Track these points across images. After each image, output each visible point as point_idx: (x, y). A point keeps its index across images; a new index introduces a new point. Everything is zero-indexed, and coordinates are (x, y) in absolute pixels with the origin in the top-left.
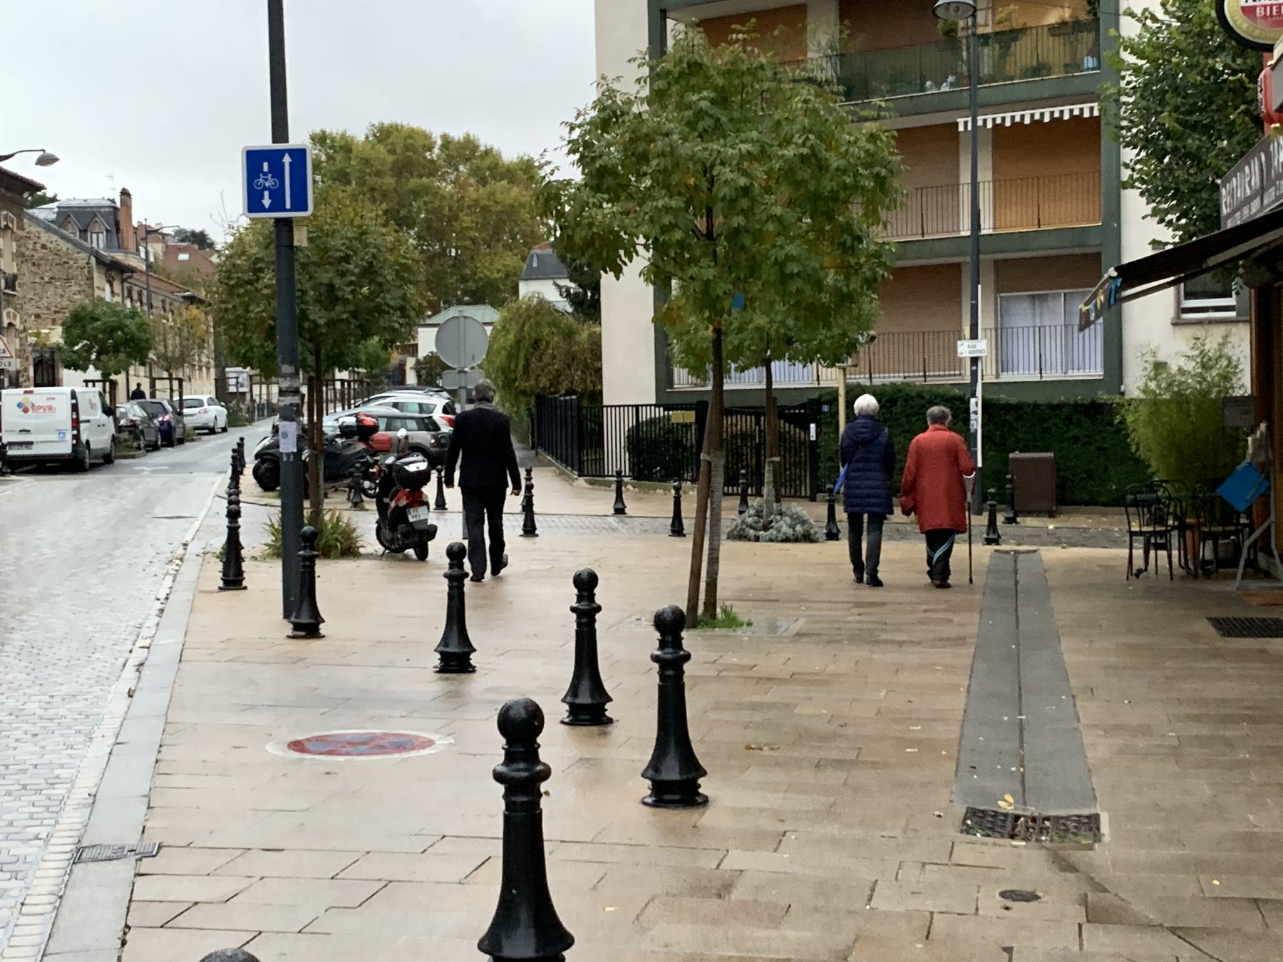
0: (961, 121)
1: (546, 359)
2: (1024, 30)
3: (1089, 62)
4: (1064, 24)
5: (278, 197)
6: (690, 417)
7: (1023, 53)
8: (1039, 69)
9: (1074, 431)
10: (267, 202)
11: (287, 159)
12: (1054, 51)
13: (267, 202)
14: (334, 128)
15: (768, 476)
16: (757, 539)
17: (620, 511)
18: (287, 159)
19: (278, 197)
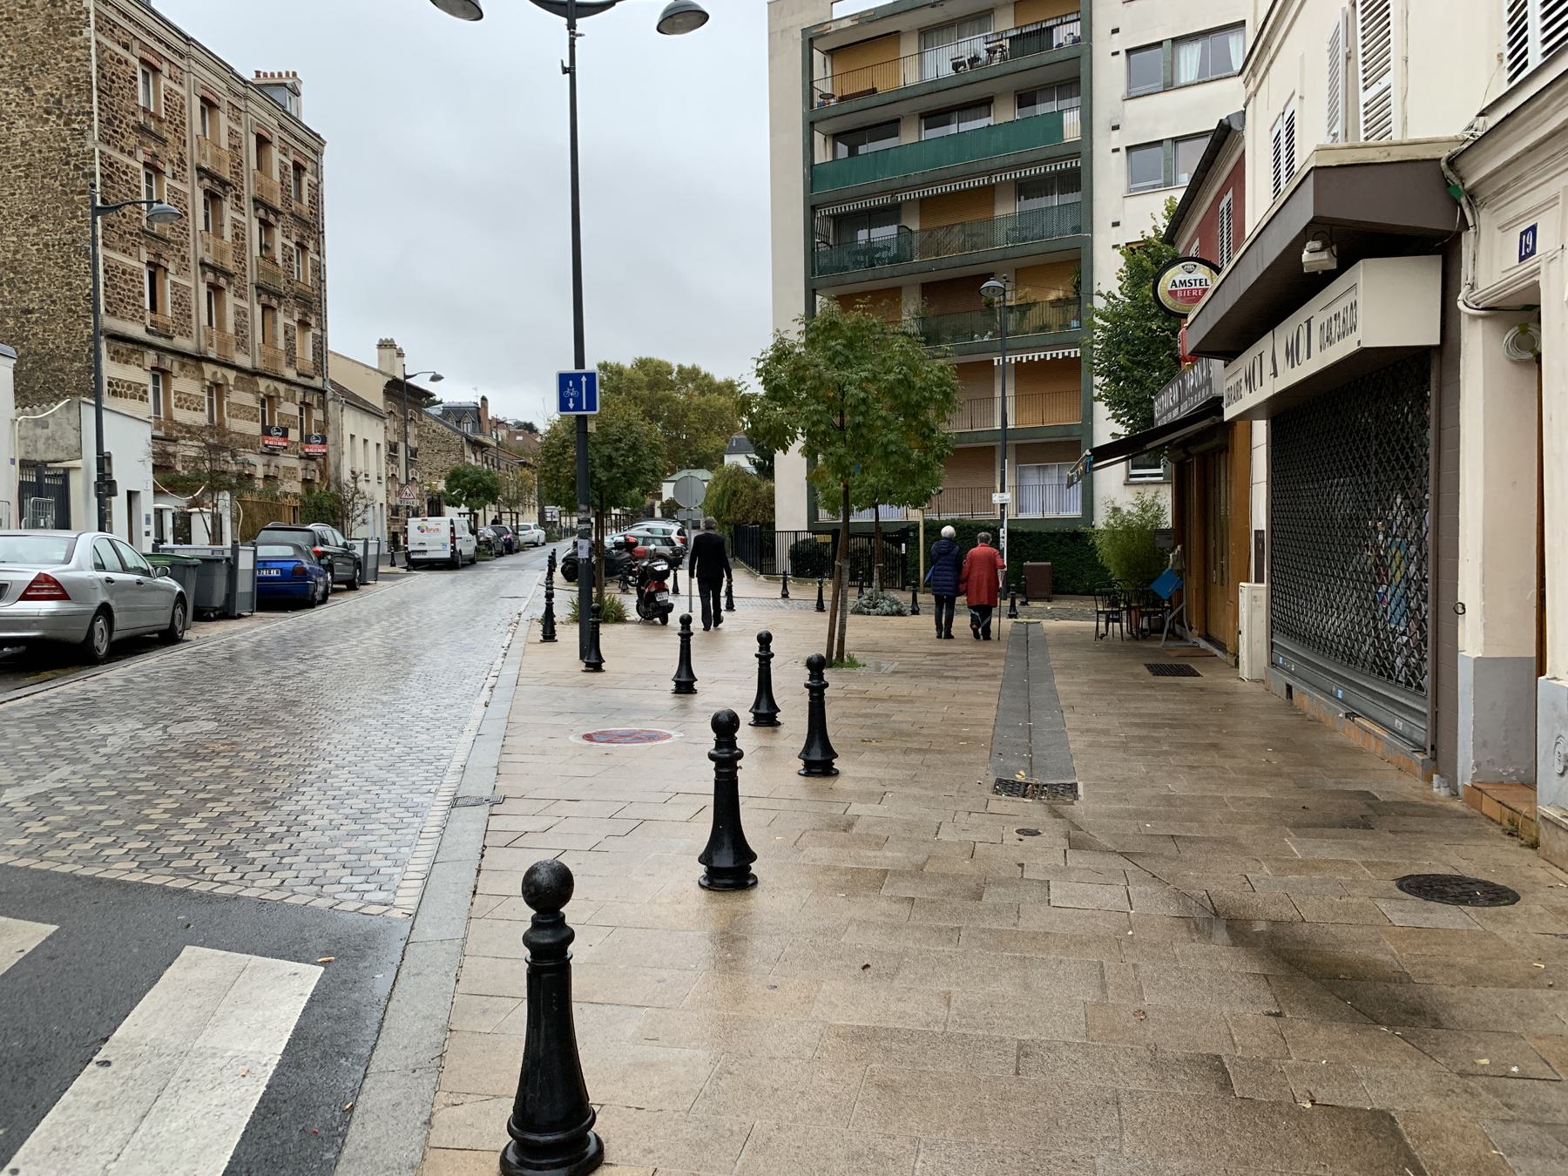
2: (1035, 304)
4: (1059, 300)
6: (828, 538)
7: (1034, 317)
8: (1043, 328)
10: (571, 405)
11: (584, 379)
12: (1052, 317)
13: (571, 405)
15: (876, 575)
18: (584, 379)
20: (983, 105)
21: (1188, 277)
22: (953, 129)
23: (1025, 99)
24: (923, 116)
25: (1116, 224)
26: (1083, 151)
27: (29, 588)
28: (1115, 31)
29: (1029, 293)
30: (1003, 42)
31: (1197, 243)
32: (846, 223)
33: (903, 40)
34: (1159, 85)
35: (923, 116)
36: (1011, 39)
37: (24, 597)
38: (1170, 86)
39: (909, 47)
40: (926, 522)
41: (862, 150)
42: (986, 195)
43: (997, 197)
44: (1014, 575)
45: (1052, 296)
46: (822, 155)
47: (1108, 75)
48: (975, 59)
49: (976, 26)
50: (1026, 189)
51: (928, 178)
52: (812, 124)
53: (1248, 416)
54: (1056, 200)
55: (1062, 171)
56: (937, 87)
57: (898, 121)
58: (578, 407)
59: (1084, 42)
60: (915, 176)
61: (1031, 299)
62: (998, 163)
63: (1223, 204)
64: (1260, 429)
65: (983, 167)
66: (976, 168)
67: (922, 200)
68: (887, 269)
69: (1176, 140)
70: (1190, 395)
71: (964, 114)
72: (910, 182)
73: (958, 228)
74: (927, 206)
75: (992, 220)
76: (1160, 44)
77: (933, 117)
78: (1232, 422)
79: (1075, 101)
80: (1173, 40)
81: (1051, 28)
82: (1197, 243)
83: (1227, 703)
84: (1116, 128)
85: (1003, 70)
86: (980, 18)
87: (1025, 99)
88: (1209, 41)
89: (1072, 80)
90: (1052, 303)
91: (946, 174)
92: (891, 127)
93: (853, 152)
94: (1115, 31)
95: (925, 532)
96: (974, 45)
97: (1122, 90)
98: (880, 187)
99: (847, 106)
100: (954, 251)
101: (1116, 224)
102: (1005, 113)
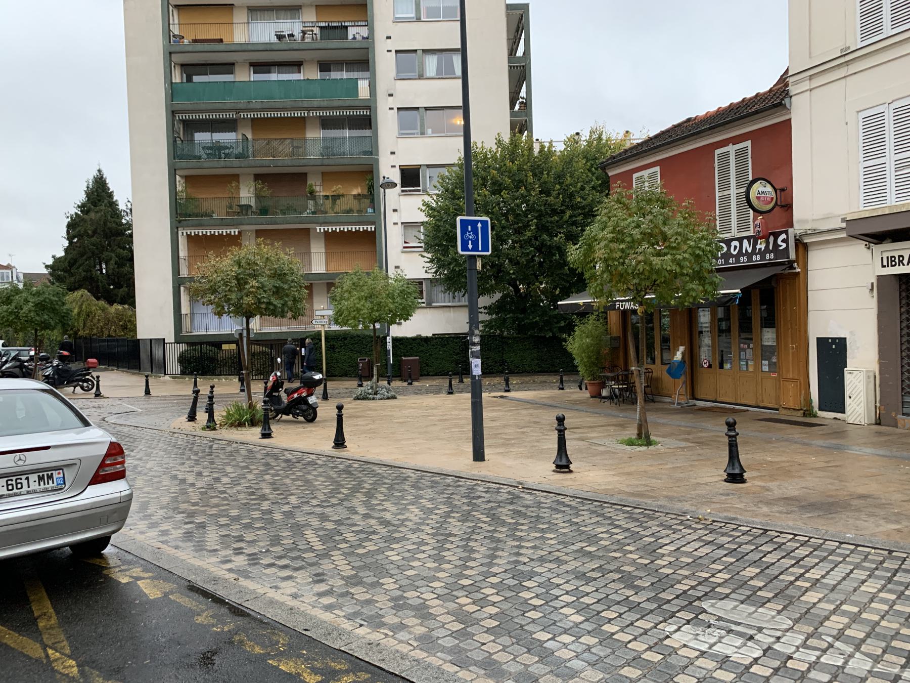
0: (318, 228)
1: (95, 321)
2: (343, 195)
3: (370, 210)
4: (359, 195)
5: (475, 243)
6: (233, 346)
7: (342, 204)
8: (350, 211)
9: (422, 348)
10: (470, 246)
11: (479, 225)
12: (354, 204)
13: (470, 246)
14: (115, 194)
15: (375, 372)
16: (374, 399)
17: (147, 392)
18: (479, 225)
19: (475, 243)
20: (297, 65)
22: (273, 77)
23: (325, 67)
24: (252, 64)
25: (393, 153)
26: (370, 106)
27: (102, 465)
28: (389, 38)
29: (337, 188)
30: (314, 29)
32: (192, 126)
33: (235, 12)
34: (416, 75)
35: (252, 64)
36: (321, 28)
37: (97, 479)
38: (421, 77)
39: (240, 16)
40: (326, 332)
41: (196, 79)
42: (300, 123)
43: (308, 126)
44: (398, 363)
45: (355, 192)
46: (177, 78)
47: (385, 64)
48: (291, 35)
49: (289, 14)
50: (327, 123)
51: (266, 106)
52: (170, 53)
54: (347, 133)
55: (350, 115)
56: (267, 48)
57: (233, 64)
59: (370, 38)
60: (256, 103)
61: (341, 192)
62: (316, 104)
65: (305, 105)
66: (300, 105)
67: (253, 120)
68: (235, 162)
69: (427, 109)
71: (284, 68)
72: (251, 106)
73: (288, 141)
74: (257, 124)
75: (305, 139)
76: (415, 51)
77: (260, 67)
79: (367, 74)
80: (424, 51)
81: (346, 27)
83: (840, 432)
84: (391, 95)
85: (190, 49)
86: (293, 10)
87: (325, 67)
88: (443, 55)
89: (363, 61)
90: (354, 196)
91: (278, 105)
92: (228, 67)
93: (189, 80)
94: (389, 38)
95: (326, 338)
96: (292, 26)
97: (393, 73)
98: (229, 106)
99: (199, 47)
100: (281, 154)
101: (393, 153)
102: (312, 73)
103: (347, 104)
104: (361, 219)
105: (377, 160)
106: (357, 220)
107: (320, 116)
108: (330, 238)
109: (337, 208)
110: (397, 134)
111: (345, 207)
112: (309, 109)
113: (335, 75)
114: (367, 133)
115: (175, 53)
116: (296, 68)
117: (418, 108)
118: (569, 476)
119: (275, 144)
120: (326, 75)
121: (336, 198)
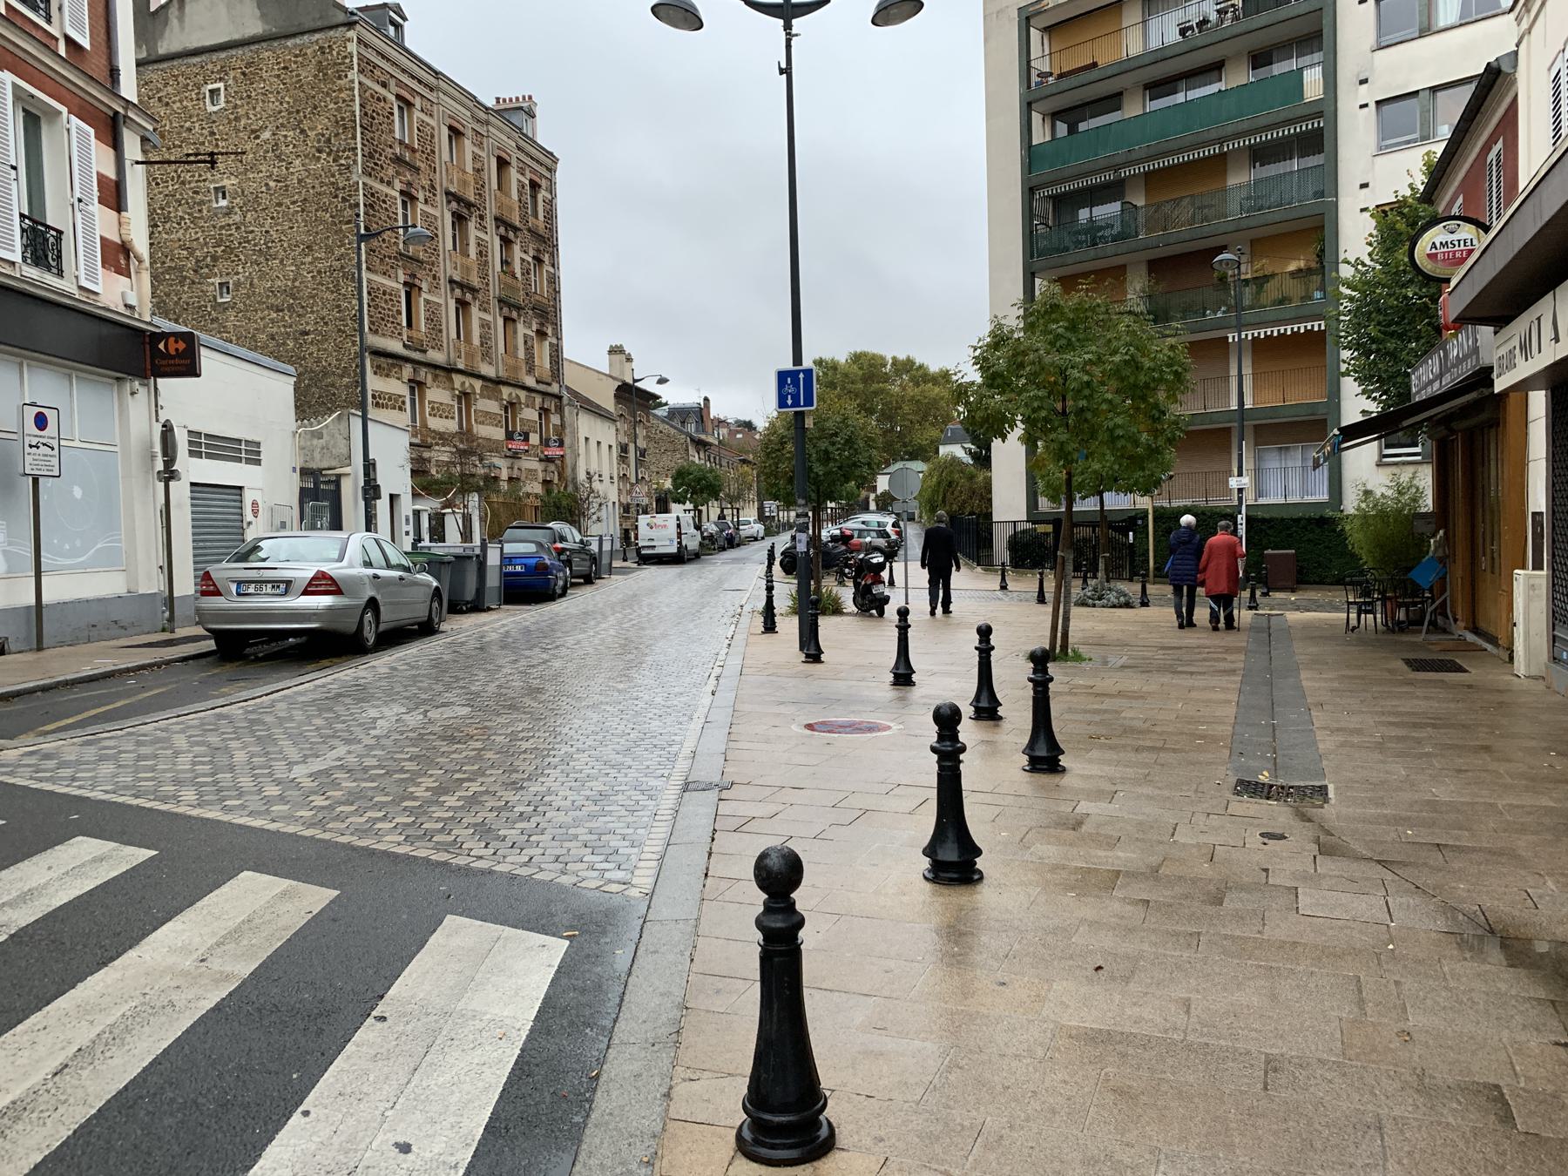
2: (1273, 275)
4: (1300, 270)
7: (1272, 290)
12: (1294, 288)
15: (1101, 566)
17: (1004, 587)
20: (1214, 69)
21: (1450, 238)
23: (1260, 59)
24: (1147, 87)
25: (1364, 186)
26: (1326, 109)
27: (310, 584)
29: (1266, 265)
31: (1460, 200)
32: (1065, 203)
35: (1147, 87)
37: (306, 593)
38: (1426, 31)
40: (1155, 510)
41: (1082, 127)
42: (1218, 165)
45: (1292, 267)
46: (1040, 135)
50: (1261, 155)
53: (1524, 386)
57: (1120, 94)
58: (796, 404)
60: (1139, 150)
62: (1230, 130)
63: (1492, 156)
64: (1538, 402)
65: (1214, 135)
66: (1207, 137)
68: (1110, 248)
69: (1434, 89)
70: (1454, 366)
72: (1134, 156)
73: (1185, 202)
77: (1160, 87)
78: (1505, 394)
79: (1317, 57)
82: (1460, 200)
84: (1364, 82)
87: (1260, 59)
90: (1292, 274)
92: (1113, 101)
99: (1066, 83)
100: (1183, 224)
101: (1364, 186)
103: (1281, 117)
104: (1306, 312)
105: (1336, 204)
106: (1293, 314)
107: (1250, 146)
108: (1264, 349)
109: (1264, 299)
110: (1373, 149)
111: (1275, 295)
112: (1221, 141)
113: (1278, 68)
114: (1313, 161)
115: (1037, 101)
116: (1216, 73)
117: (1417, 92)
118: (818, 666)
119: (1167, 209)
120: (1263, 72)
121: (1261, 281)
